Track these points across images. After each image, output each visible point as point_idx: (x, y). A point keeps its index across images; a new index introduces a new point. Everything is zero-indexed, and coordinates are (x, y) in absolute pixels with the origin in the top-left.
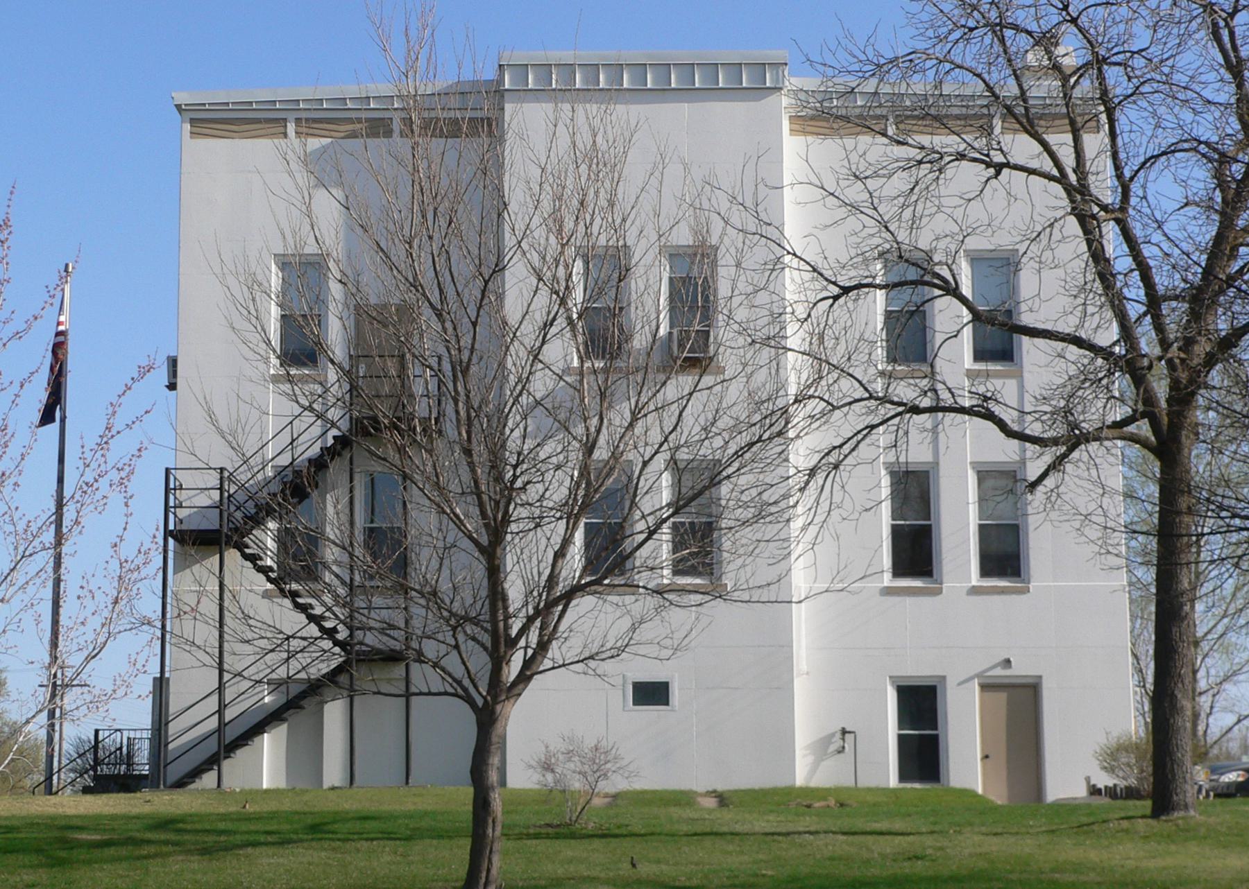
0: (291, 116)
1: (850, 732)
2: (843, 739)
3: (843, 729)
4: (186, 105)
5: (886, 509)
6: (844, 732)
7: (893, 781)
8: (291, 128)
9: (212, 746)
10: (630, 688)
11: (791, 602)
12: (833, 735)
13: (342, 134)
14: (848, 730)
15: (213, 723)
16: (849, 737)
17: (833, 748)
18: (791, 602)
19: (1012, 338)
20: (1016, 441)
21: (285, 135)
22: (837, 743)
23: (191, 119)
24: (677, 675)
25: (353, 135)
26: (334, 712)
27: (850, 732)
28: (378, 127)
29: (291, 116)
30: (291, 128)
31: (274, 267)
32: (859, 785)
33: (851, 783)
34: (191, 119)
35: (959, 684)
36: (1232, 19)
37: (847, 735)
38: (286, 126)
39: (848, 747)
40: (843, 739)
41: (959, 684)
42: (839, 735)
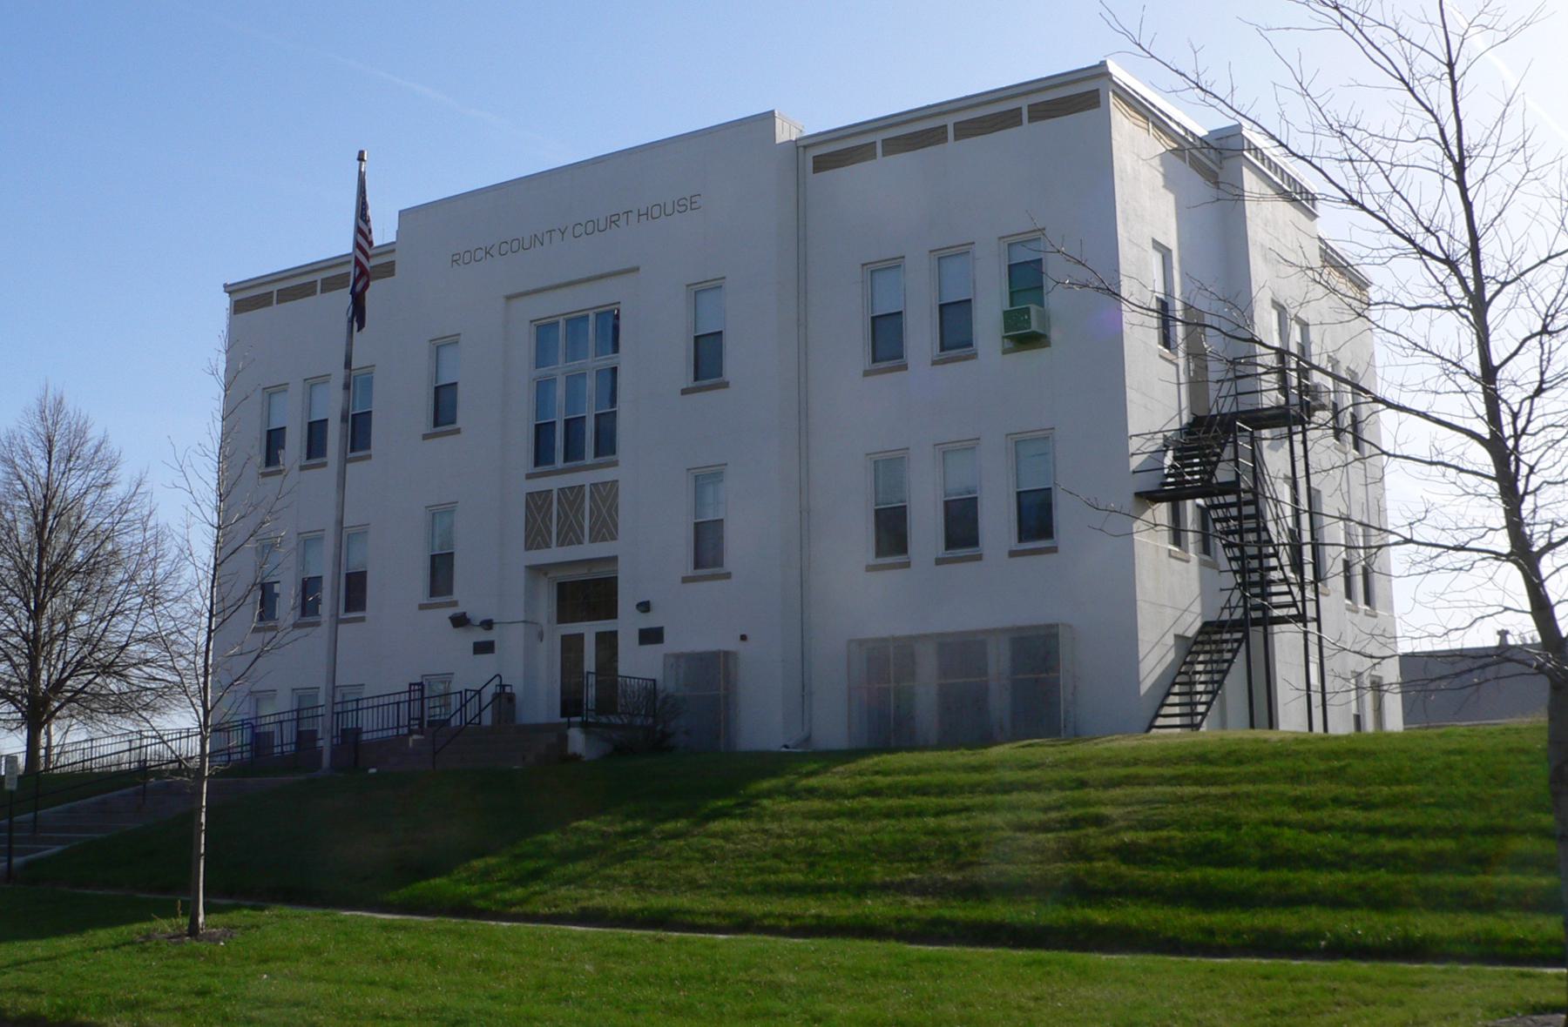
11: (524, 622)
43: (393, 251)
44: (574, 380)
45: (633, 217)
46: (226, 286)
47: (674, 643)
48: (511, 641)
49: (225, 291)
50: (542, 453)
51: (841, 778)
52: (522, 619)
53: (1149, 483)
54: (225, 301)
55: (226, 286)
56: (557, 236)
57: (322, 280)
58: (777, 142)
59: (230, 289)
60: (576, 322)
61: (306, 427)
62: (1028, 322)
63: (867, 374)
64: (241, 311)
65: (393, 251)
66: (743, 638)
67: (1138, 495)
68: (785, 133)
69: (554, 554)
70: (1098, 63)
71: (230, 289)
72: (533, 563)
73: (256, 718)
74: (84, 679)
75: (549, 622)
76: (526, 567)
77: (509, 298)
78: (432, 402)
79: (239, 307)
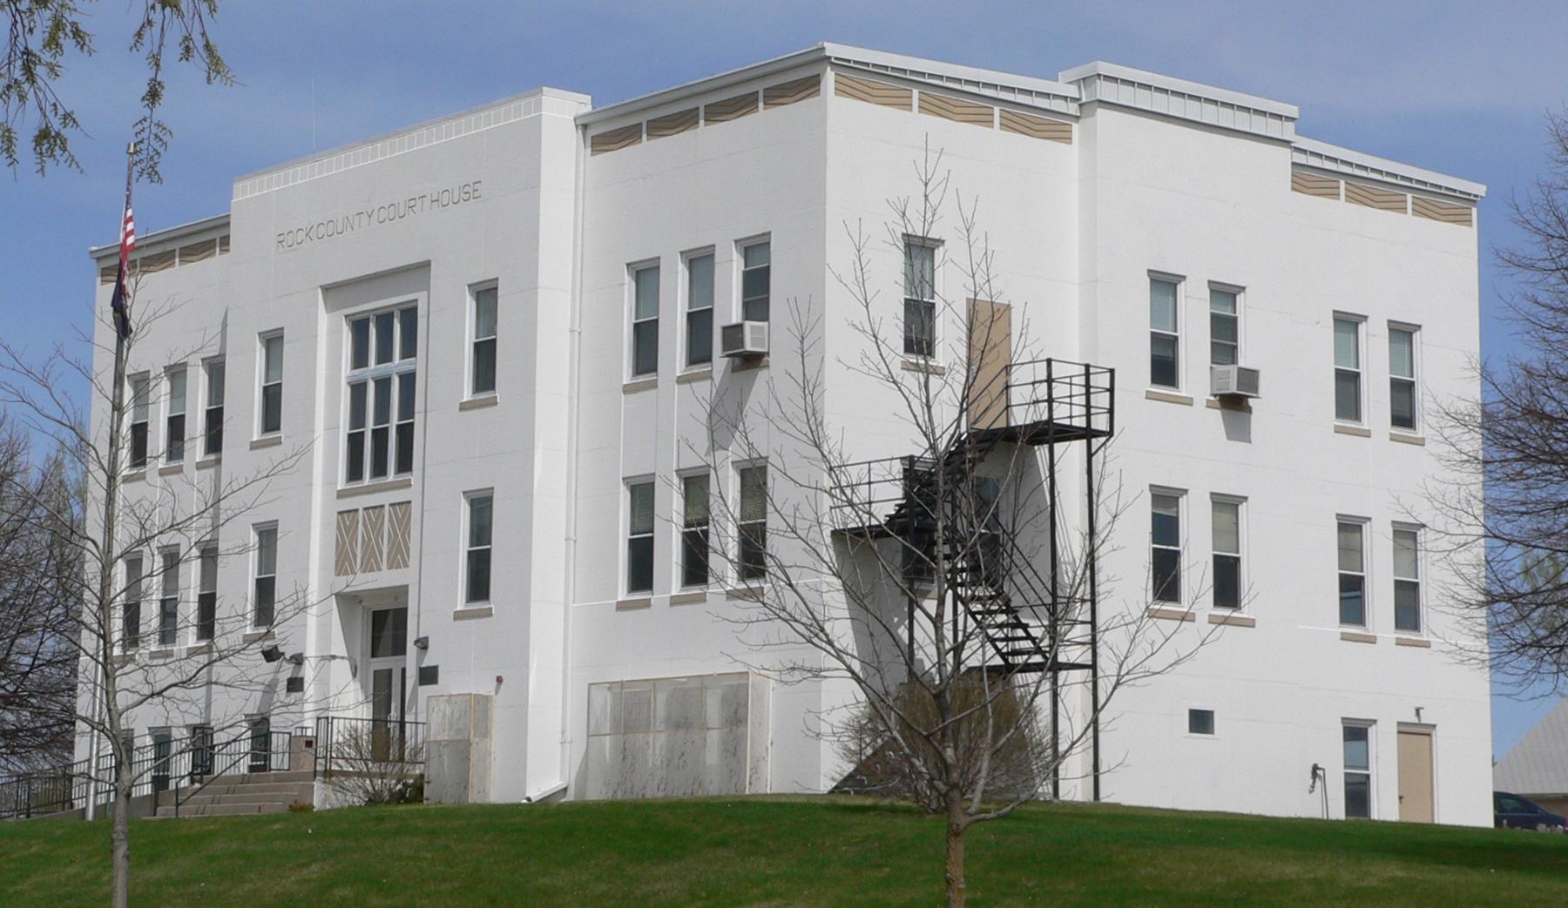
4: (836, 58)
14: (1320, 766)
44: (383, 385)
45: (427, 201)
47: (448, 683)
50: (355, 472)
56: (364, 217)
60: (384, 321)
62: (742, 341)
69: (364, 581)
75: (362, 655)
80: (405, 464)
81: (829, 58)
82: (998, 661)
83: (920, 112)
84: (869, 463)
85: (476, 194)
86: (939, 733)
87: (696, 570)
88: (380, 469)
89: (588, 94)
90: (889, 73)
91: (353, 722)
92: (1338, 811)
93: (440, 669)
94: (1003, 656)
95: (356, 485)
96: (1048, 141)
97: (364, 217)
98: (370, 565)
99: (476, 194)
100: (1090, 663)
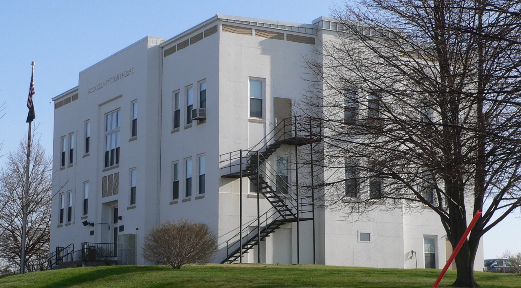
0: (254, 28)
1: (414, 252)
2: (412, 254)
3: (412, 251)
4: (222, 19)
5: (75, 268)
6: (413, 252)
7: (424, 268)
8: (254, 32)
9: (237, 246)
10: (359, 234)
11: (102, 223)
12: (409, 253)
13: (269, 37)
14: (413, 251)
15: (238, 238)
16: (414, 254)
17: (409, 257)
18: (102, 223)
19: (220, 250)
20: (257, 224)
21: (252, 34)
22: (410, 255)
23: (223, 24)
24: (372, 231)
25: (273, 38)
26: (269, 240)
27: (414, 252)
28: (279, 36)
29: (254, 28)
30: (254, 32)
31: (249, 81)
32: (418, 268)
33: (415, 267)
34: (223, 24)
35: (441, 238)
36: (242, 254)
37: (413, 253)
38: (252, 31)
39: (414, 257)
40: (412, 254)
41: (441, 238)
42: (411, 253)
43: (78, 89)
46: (52, 99)
47: (126, 231)
48: (98, 229)
49: (53, 101)
50: (106, 165)
51: (407, 180)
52: (101, 222)
53: (227, 172)
54: (53, 103)
55: (52, 99)
57: (73, 96)
58: (148, 47)
59: (54, 99)
61: (85, 139)
63: (172, 132)
64: (57, 108)
65: (78, 89)
66: (137, 229)
67: (222, 177)
68: (153, 43)
70: (215, 15)
71: (54, 99)
72: (105, 202)
73: (247, 158)
74: (391, 37)
75: (111, 223)
76: (102, 204)
77: (100, 105)
78: (85, 147)
79: (57, 106)
80: (117, 162)
81: (220, 19)
82: (281, 218)
83: (255, 36)
84: (230, 153)
85: (133, 72)
86: (35, 250)
87: (188, 193)
88: (112, 164)
89: (268, 54)
90: (243, 23)
91: (94, 244)
92: (422, 265)
93: (124, 227)
94: (283, 216)
95: (107, 168)
96: (243, 35)
97: (108, 81)
98: (109, 195)
99: (133, 72)
100: (312, 218)
